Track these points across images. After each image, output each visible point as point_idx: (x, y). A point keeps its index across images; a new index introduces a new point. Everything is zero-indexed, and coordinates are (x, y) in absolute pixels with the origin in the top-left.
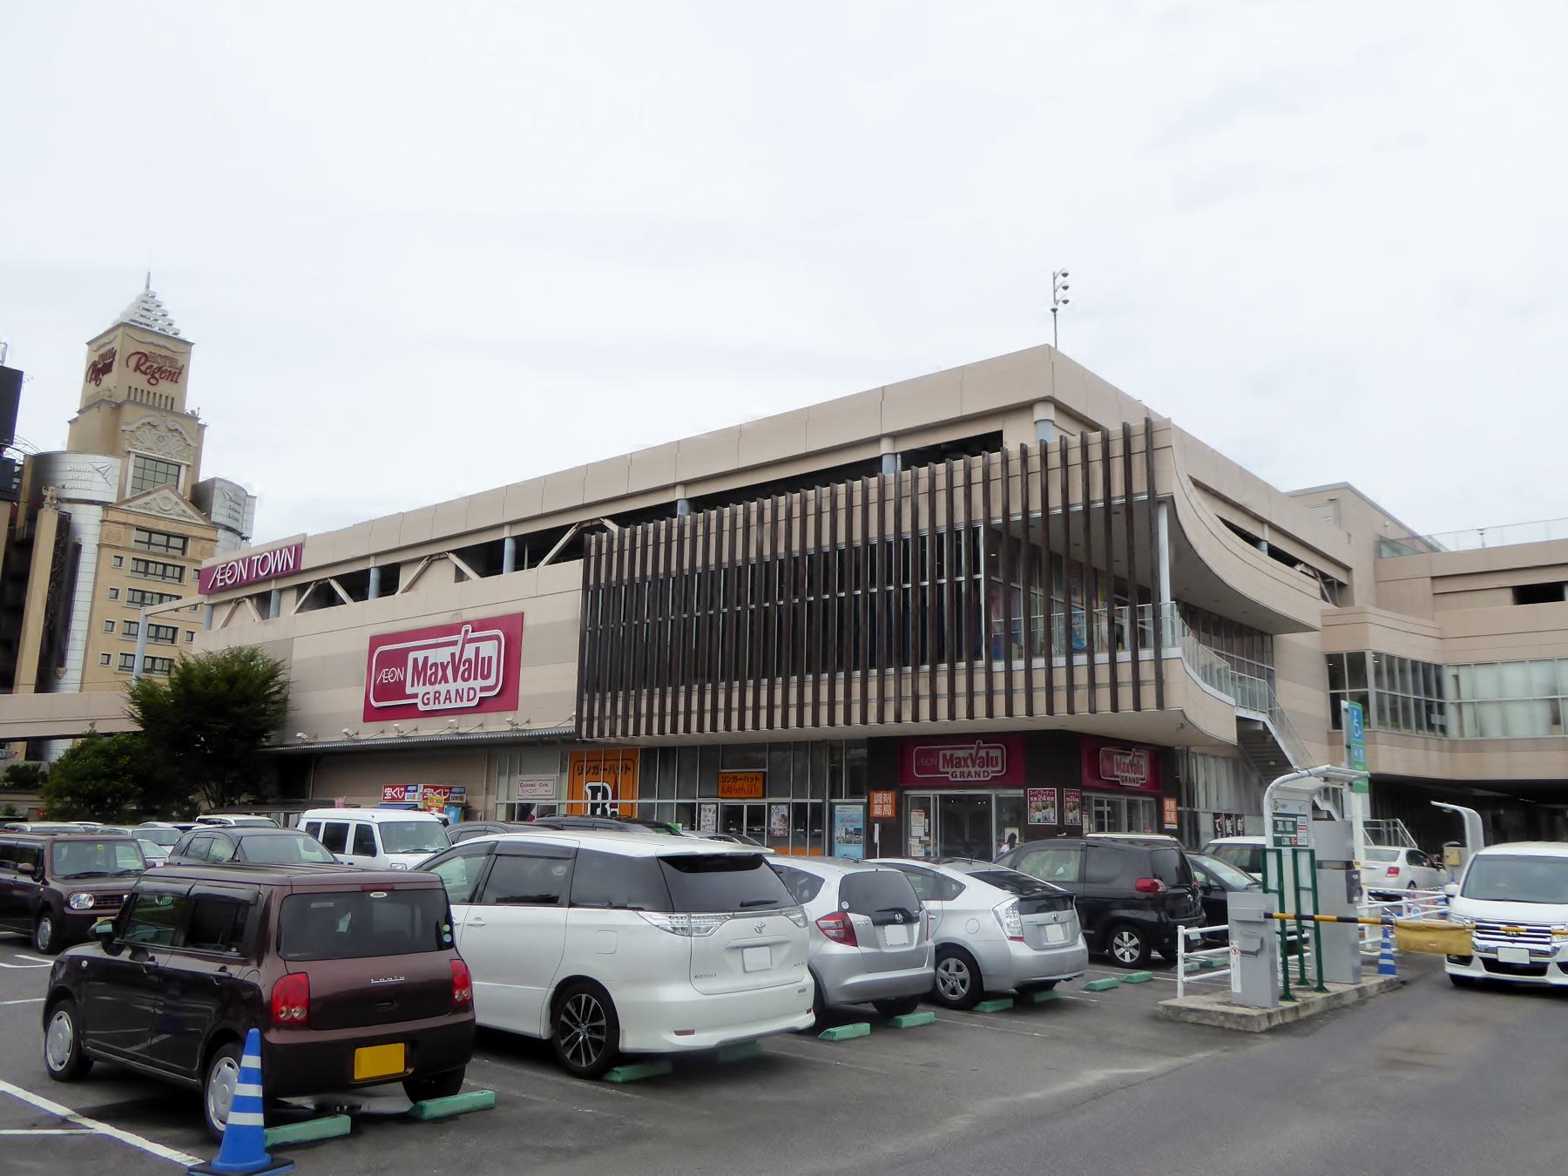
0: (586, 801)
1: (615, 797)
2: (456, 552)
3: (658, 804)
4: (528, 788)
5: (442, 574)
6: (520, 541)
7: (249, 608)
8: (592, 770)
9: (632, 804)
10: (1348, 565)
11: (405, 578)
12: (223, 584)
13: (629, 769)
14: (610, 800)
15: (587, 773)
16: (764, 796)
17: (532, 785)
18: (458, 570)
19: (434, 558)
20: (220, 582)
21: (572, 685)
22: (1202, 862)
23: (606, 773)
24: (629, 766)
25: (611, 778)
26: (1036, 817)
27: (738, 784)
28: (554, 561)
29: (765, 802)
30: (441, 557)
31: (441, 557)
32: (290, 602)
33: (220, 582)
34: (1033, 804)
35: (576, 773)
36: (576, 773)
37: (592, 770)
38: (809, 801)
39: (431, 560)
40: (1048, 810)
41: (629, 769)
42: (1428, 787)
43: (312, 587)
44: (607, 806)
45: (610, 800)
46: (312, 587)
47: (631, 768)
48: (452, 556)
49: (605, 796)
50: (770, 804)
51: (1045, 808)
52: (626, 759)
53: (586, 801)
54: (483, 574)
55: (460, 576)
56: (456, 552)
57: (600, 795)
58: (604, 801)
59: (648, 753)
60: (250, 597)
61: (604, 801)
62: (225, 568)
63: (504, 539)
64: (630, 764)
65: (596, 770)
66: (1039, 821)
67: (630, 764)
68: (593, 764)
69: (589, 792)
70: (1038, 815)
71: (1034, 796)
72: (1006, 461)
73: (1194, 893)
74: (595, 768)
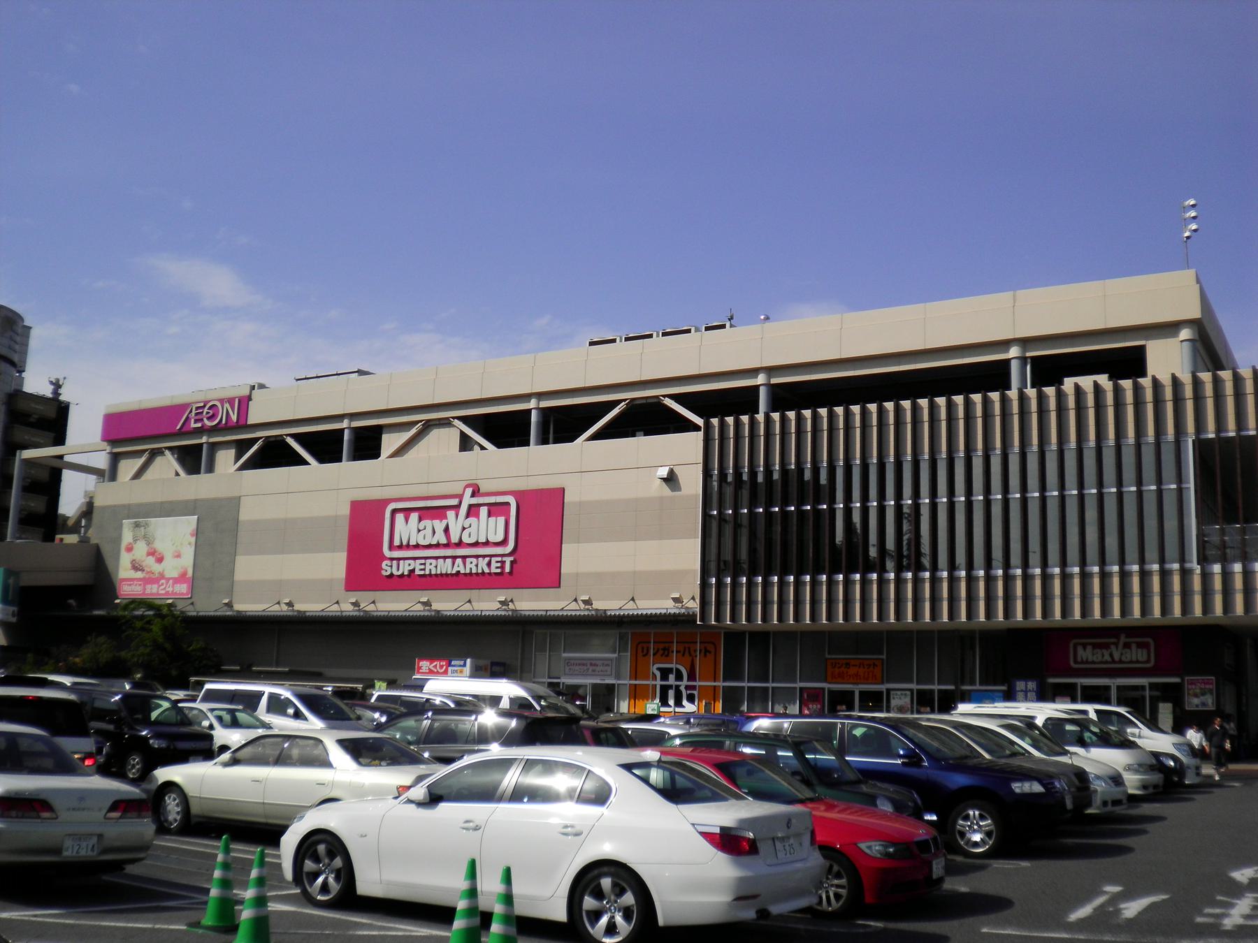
0: (654, 683)
1: (692, 677)
2: (464, 419)
3: (773, 688)
4: (577, 668)
5: (444, 441)
6: (546, 413)
7: (168, 464)
8: (661, 652)
9: (715, 687)
10: (561, 585)
11: (390, 442)
12: (199, 425)
13: (710, 652)
14: (685, 682)
15: (654, 655)
16: (882, 683)
17: (583, 665)
18: (463, 436)
19: (431, 423)
20: (195, 423)
21: (693, 561)
22: (737, 834)
23: (678, 654)
24: (708, 648)
25: (688, 658)
26: (1193, 703)
27: (852, 671)
28: (596, 437)
29: (883, 687)
30: (442, 422)
31: (445, 423)
32: (226, 460)
33: (195, 423)
34: (1191, 692)
35: (640, 654)
36: (640, 654)
37: (661, 652)
38: (936, 687)
39: (428, 426)
40: (1206, 697)
41: (710, 652)
42: (149, 887)
43: (260, 442)
44: (682, 688)
45: (685, 682)
46: (260, 442)
47: (713, 651)
48: (456, 422)
49: (679, 677)
50: (888, 691)
51: (1203, 694)
52: (705, 643)
53: (654, 683)
54: (322, 460)
55: (466, 444)
56: (464, 419)
57: (672, 677)
58: (678, 683)
59: (734, 638)
60: (170, 448)
61: (678, 683)
62: (204, 406)
63: (531, 409)
64: (710, 647)
65: (665, 653)
66: (1197, 706)
67: (710, 647)
68: (661, 646)
69: (658, 674)
70: (1196, 701)
71: (1192, 684)
72: (1237, 379)
73: (980, 826)
74: (664, 649)
